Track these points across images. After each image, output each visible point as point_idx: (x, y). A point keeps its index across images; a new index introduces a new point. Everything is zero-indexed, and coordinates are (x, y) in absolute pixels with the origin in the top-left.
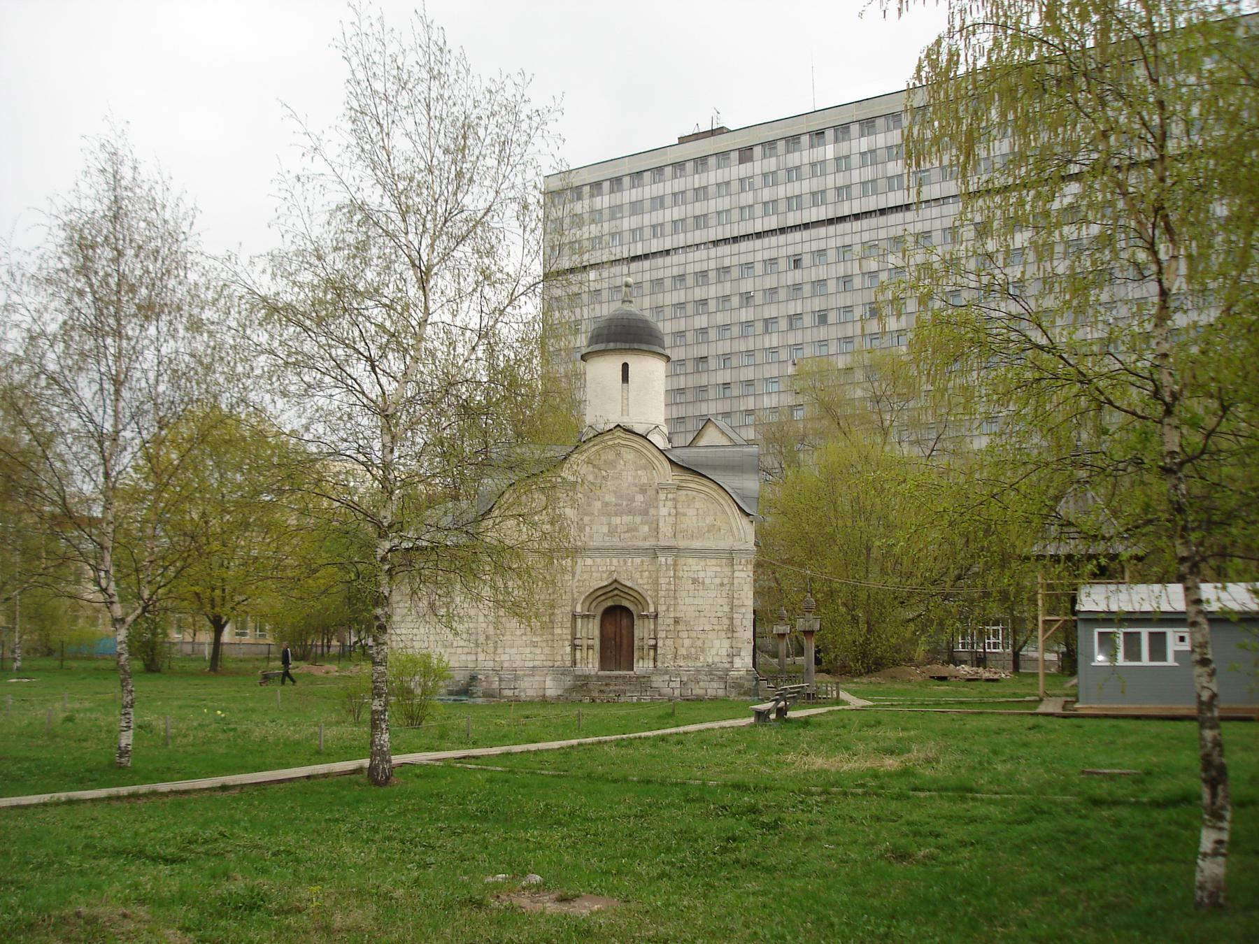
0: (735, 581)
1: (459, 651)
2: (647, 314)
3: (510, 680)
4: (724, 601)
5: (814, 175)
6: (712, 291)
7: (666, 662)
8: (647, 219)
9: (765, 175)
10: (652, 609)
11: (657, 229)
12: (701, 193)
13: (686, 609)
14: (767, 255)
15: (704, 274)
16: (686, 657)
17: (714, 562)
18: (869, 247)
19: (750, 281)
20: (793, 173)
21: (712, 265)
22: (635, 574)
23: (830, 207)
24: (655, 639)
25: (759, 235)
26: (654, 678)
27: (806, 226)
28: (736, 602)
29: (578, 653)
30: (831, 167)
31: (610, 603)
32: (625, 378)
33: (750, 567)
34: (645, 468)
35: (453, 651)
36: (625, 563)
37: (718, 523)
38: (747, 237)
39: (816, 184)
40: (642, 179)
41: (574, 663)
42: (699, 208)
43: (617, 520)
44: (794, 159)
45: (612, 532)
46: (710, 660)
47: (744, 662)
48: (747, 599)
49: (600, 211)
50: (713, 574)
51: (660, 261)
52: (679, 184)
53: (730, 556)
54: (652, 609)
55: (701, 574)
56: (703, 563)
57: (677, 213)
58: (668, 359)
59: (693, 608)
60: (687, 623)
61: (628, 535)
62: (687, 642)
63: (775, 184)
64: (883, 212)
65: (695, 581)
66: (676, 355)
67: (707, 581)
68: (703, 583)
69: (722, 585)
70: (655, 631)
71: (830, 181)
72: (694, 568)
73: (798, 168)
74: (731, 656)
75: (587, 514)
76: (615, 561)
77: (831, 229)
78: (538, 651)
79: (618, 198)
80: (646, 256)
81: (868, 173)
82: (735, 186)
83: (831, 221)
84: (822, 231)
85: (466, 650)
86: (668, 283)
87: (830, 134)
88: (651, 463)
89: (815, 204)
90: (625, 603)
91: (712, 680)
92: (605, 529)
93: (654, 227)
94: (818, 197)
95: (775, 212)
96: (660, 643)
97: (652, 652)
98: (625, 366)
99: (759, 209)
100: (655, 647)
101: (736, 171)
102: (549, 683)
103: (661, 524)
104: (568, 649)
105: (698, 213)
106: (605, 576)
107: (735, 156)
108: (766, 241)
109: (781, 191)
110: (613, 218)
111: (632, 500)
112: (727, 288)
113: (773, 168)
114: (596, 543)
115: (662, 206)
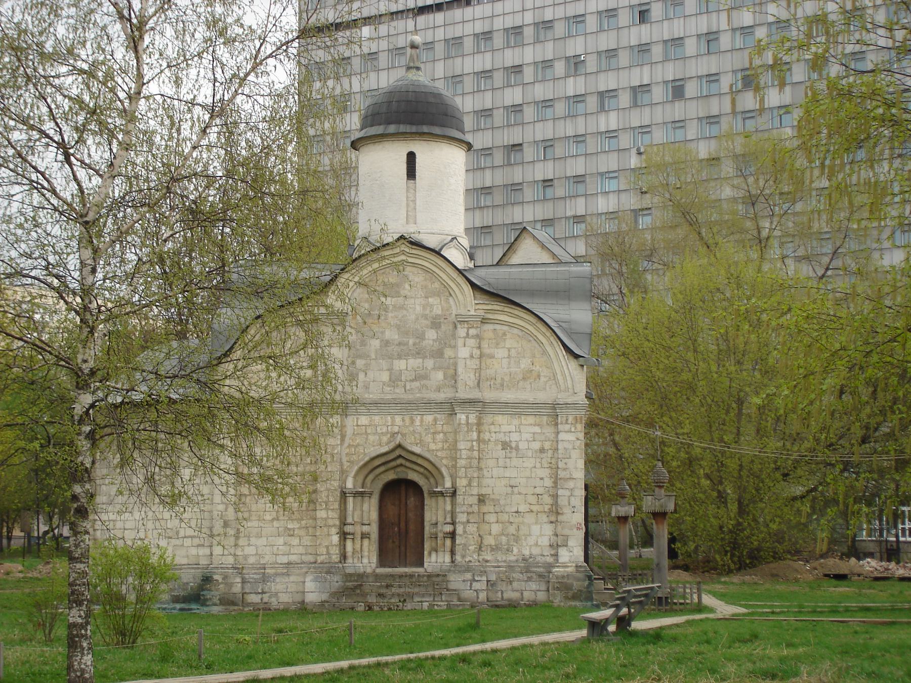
1: (188, 542)
6: (529, 55)
7: (468, 554)
15: (517, 31)
16: (495, 549)
17: (531, 420)
19: (580, 40)
22: (425, 436)
24: (453, 523)
26: (452, 577)
29: (349, 544)
31: (391, 476)
32: (411, 173)
33: (580, 427)
34: (438, 294)
35: (178, 542)
36: (412, 421)
37: (537, 368)
41: (344, 557)
43: (400, 365)
45: (395, 379)
46: (527, 552)
47: (572, 555)
55: (515, 437)
56: (516, 422)
60: (496, 502)
61: (417, 384)
62: (496, 529)
65: (506, 445)
67: (522, 446)
68: (517, 448)
69: (542, 450)
70: (453, 513)
72: (505, 428)
74: (555, 546)
76: (398, 419)
78: (295, 541)
86: (468, 43)
90: (412, 476)
91: (530, 579)
92: (385, 377)
96: (460, 530)
98: (411, 157)
100: (453, 535)
102: (310, 585)
103: (460, 370)
104: (335, 539)
106: (385, 439)
111: (421, 337)
112: (548, 51)
114: (373, 395)
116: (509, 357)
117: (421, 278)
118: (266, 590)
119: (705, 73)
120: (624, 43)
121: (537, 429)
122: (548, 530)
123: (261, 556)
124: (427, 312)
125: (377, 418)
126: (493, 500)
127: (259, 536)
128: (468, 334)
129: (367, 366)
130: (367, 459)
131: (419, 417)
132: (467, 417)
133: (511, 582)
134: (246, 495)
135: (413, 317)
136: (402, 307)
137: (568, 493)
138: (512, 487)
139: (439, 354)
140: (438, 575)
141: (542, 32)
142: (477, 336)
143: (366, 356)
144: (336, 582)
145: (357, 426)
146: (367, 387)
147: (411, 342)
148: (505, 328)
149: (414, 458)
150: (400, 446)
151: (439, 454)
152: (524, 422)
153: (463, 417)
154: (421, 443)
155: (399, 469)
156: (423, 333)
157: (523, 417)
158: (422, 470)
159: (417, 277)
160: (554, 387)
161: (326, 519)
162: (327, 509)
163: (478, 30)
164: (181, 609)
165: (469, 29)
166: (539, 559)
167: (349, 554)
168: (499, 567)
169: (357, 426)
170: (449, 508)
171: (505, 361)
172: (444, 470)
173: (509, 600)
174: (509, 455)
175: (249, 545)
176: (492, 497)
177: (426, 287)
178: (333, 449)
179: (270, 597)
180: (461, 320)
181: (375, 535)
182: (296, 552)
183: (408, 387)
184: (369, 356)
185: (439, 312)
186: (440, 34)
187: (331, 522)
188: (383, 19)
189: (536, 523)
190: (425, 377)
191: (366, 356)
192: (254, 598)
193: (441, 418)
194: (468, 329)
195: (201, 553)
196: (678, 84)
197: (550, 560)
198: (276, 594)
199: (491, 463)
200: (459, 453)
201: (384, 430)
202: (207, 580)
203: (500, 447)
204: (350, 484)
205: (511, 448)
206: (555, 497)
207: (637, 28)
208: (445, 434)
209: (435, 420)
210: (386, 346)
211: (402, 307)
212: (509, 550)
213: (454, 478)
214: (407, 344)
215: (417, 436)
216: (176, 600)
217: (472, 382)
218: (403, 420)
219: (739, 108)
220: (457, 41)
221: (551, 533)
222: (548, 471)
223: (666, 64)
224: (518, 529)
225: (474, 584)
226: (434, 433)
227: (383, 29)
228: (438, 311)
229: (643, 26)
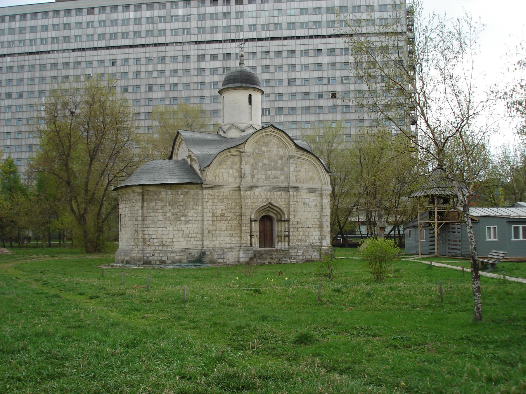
1: (193, 239)
3: (221, 254)
5: (124, 24)
6: (71, 72)
7: (294, 243)
8: (39, 35)
9: (100, 22)
11: (44, 41)
12: (67, 26)
13: (302, 219)
15: (67, 64)
16: (301, 240)
17: (313, 194)
18: (149, 60)
19: (91, 69)
20: (114, 23)
21: (72, 60)
22: (279, 199)
23: (131, 40)
24: (289, 232)
25: (95, 49)
26: (291, 251)
27: (119, 47)
29: (253, 239)
30: (132, 22)
31: (264, 214)
32: (250, 102)
33: (329, 197)
34: (281, 147)
35: (189, 239)
37: (314, 176)
38: (90, 49)
39: (124, 29)
40: (37, 16)
42: (66, 33)
43: (269, 173)
44: (114, 16)
45: (267, 178)
46: (311, 242)
47: (327, 242)
48: (328, 211)
49: (14, 29)
50: (312, 200)
51: (45, 56)
52: (56, 21)
53: (321, 192)
54: (286, 217)
55: (307, 200)
56: (308, 195)
57: (54, 34)
58: (263, 92)
60: (301, 224)
61: (275, 180)
62: (301, 233)
63: (104, 26)
64: (156, 45)
65: (305, 204)
66: (267, 90)
67: (310, 204)
68: (308, 205)
69: (316, 205)
71: (131, 28)
72: (304, 197)
73: (116, 20)
74: (321, 239)
75: (255, 169)
76: (269, 193)
77: (131, 50)
78: (233, 239)
79: (23, 24)
80: (38, 53)
81: (150, 27)
82: (84, 25)
83: (131, 46)
84: (127, 50)
85: (196, 239)
86: (49, 67)
87: (132, 7)
88: (285, 145)
89: (123, 38)
90: (271, 214)
91: (314, 251)
92: (264, 177)
93: (42, 39)
94: (125, 35)
96: (291, 234)
97: (287, 238)
98: (250, 96)
99: (96, 37)
100: (289, 236)
101: (85, 18)
102: (242, 255)
103: (291, 176)
104: (249, 237)
105: (65, 35)
106: (264, 200)
107: (85, 11)
109: (108, 30)
110: (21, 32)
111: (276, 163)
112: (79, 71)
113: (104, 19)
114: (260, 184)
115: (47, 30)
120: (60, 74)
122: (318, 233)
123: (221, 244)
125: (261, 192)
129: (258, 172)
136: (269, 151)
139: (282, 169)
141: (76, 65)
142: (296, 164)
146: (258, 181)
149: (274, 208)
150: (270, 203)
153: (292, 193)
154: (277, 202)
156: (277, 161)
158: (275, 212)
159: (275, 141)
161: (245, 230)
162: (246, 226)
163: (52, 62)
165: (49, 62)
166: (315, 244)
170: (287, 226)
180: (289, 158)
181: (258, 236)
186: (38, 62)
187: (247, 231)
188: (16, 55)
192: (220, 261)
197: (319, 244)
199: (300, 210)
209: (282, 194)
211: (269, 151)
212: (306, 241)
213: (289, 215)
214: (271, 165)
216: (190, 262)
217: (294, 180)
220: (44, 65)
227: (16, 58)
228: (282, 153)
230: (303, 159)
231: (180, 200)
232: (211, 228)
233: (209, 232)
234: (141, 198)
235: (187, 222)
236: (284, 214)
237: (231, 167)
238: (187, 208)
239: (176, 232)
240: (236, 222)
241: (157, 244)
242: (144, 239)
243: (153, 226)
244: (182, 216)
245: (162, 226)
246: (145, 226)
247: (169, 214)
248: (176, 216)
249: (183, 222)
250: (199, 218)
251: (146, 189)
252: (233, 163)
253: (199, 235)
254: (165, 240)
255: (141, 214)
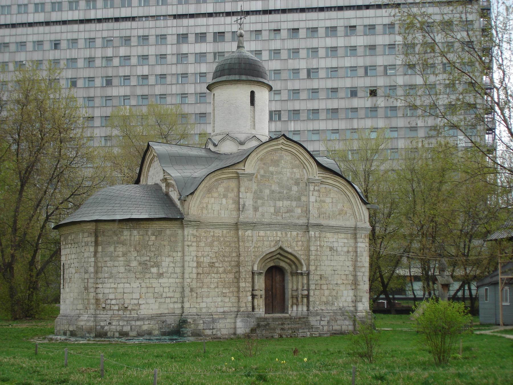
0: (358, 250)
1: (168, 300)
2: (253, 56)
4: (349, 263)
7: (316, 306)
10: (305, 269)
14: (36, 38)
16: (326, 303)
17: (343, 236)
23: (82, 13)
24: (308, 290)
25: (30, 25)
27: (64, 22)
28: (359, 264)
29: (256, 301)
31: (272, 264)
33: (367, 240)
34: (298, 167)
35: (163, 300)
36: (286, 234)
37: (345, 209)
38: (22, 25)
41: (253, 308)
43: (280, 204)
45: (277, 212)
46: (341, 305)
48: (365, 260)
53: (355, 231)
54: (305, 269)
55: (335, 244)
56: (336, 237)
59: (331, 268)
60: (327, 279)
61: (288, 214)
62: (327, 293)
64: (117, 20)
65: (331, 249)
67: (339, 249)
68: (337, 251)
69: (348, 252)
70: (308, 285)
72: (331, 240)
75: (259, 198)
76: (279, 233)
77: (82, 26)
78: (227, 300)
83: (82, 22)
84: (75, 27)
85: (173, 300)
89: (71, 9)
90: (282, 264)
91: (345, 319)
92: (272, 210)
95: (43, 11)
96: (312, 293)
97: (305, 300)
98: (252, 93)
100: (308, 296)
102: (239, 324)
104: (250, 298)
106: (273, 244)
108: (36, 29)
111: (290, 189)
114: (266, 220)
116: (332, 202)
117: (290, 158)
118: (215, 327)
119: (87, 76)
121: (346, 241)
122: (351, 293)
124: (293, 176)
125: (268, 232)
126: (325, 277)
127: (208, 297)
128: (314, 189)
130: (264, 254)
131: (289, 233)
132: (315, 233)
133: (336, 321)
134: (201, 274)
135: (286, 178)
136: (280, 173)
137: (362, 274)
138: (334, 270)
139: (299, 199)
140: (304, 318)
143: (263, 198)
144: (253, 323)
145: (259, 236)
147: (285, 192)
148: (331, 187)
149: (286, 255)
151: (299, 253)
152: (339, 236)
153: (313, 233)
154: (290, 246)
155: (276, 261)
156: (291, 188)
157: (339, 234)
158: (288, 261)
159: (288, 157)
160: (353, 219)
161: (245, 287)
162: (245, 282)
164: (169, 339)
166: (347, 308)
167: (256, 307)
168: (330, 313)
169: (259, 236)
170: (305, 281)
171: (330, 204)
172: (303, 261)
173: (336, 330)
174: (333, 254)
175: (203, 302)
176: (325, 276)
177: (292, 163)
178: (248, 249)
179: (217, 331)
180: (309, 182)
181: (264, 296)
182: (227, 306)
183: (284, 216)
184: (264, 198)
185: (299, 177)
189: (346, 290)
190: (292, 211)
191: (263, 198)
193: (301, 233)
194: (315, 186)
195: (176, 307)
196: (108, 78)
198: (220, 329)
199: (324, 258)
200: (311, 252)
201: (272, 239)
202: (183, 322)
203: (328, 249)
204: (255, 268)
205: (334, 250)
206: (355, 276)
207: (54, 51)
208: (302, 242)
209: (298, 234)
210: (272, 193)
211: (280, 173)
212: (333, 304)
213: (308, 265)
214: (283, 193)
215: (289, 243)
218: (282, 234)
219: (428, 83)
221: (352, 295)
222: (351, 262)
223: (68, 70)
224: (337, 293)
225: (321, 322)
226: (297, 241)
228: (298, 176)
229: (56, 51)
230: (329, 184)
231: (151, 243)
232: (194, 285)
233: (192, 290)
234: (93, 239)
235: (160, 275)
236: (302, 265)
237: (225, 196)
238: (160, 255)
239: (144, 290)
240: (231, 276)
241: (116, 307)
242: (97, 300)
243: (111, 280)
244: (152, 267)
245: (124, 280)
246: (99, 281)
247: (134, 264)
248: (145, 266)
249: (155, 276)
250: (178, 270)
251: (102, 226)
252: (227, 189)
253: (178, 295)
254: (127, 301)
255: (93, 264)
